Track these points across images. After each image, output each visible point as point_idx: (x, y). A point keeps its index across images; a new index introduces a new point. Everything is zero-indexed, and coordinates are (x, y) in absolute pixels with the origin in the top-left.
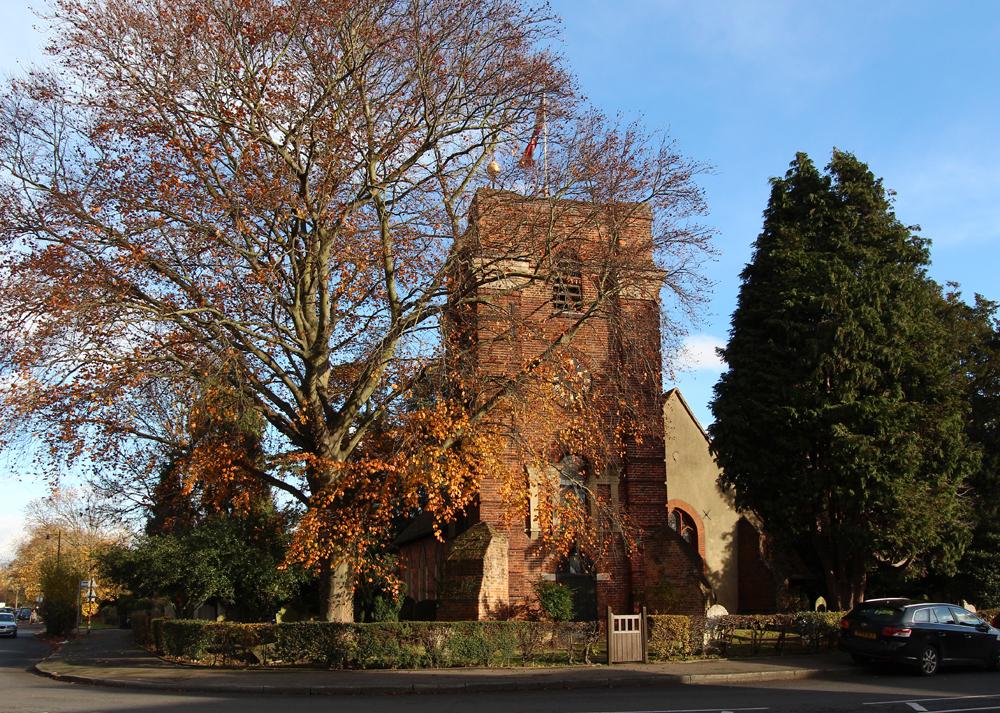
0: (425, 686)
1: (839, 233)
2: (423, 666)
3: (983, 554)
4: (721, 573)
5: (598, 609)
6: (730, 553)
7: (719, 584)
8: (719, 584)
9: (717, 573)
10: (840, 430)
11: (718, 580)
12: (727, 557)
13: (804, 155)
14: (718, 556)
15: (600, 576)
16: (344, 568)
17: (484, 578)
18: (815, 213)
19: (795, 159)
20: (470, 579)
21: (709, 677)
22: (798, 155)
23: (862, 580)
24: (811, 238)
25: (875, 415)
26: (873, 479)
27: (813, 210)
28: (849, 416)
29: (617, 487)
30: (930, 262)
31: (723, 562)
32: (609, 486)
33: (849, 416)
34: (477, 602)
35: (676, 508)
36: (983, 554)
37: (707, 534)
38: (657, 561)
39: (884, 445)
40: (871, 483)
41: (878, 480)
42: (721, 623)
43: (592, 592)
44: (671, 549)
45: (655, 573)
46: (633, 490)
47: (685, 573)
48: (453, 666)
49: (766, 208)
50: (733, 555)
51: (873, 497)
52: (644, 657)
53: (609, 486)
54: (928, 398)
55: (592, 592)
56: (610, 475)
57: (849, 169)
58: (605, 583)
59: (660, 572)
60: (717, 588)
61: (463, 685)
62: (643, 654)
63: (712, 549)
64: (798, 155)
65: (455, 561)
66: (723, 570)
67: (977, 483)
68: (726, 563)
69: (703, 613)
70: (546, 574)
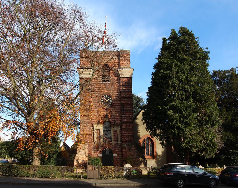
0: (15, 182)
1: (179, 53)
2: (33, 177)
3: (234, 151)
4: (161, 155)
5: (114, 164)
6: (164, 150)
7: (160, 158)
8: (160, 158)
9: (159, 156)
10: (170, 112)
11: (160, 157)
12: (163, 151)
13: (174, 30)
14: (160, 150)
15: (114, 155)
16: (36, 151)
17: (77, 155)
18: (173, 47)
19: (171, 31)
20: (74, 155)
21: (102, 184)
22: (172, 30)
23: (187, 158)
24: (172, 54)
25: (181, 107)
26: (178, 127)
27: (172, 46)
28: (174, 108)
29: (119, 130)
30: (209, 59)
31: (161, 152)
32: (117, 130)
33: (174, 108)
34: (74, 161)
35: (147, 137)
36: (234, 151)
37: (157, 144)
38: (130, 151)
39: (184, 117)
40: (178, 128)
41: (180, 127)
42: (129, 169)
43: (112, 159)
44: (133, 148)
45: (129, 155)
46: (123, 131)
47: (136, 155)
48: (41, 177)
49: (161, 47)
50: (165, 150)
51: (179, 132)
52: (99, 178)
53: (117, 130)
54: (201, 102)
55: (112, 159)
56: (117, 127)
57: (184, 32)
58: (116, 157)
59: (130, 154)
60: (160, 159)
61: (24, 183)
62: (99, 177)
63: (158, 148)
64: (172, 30)
65: (71, 150)
66: (162, 154)
67: (226, 127)
68: (163, 152)
69: (123, 166)
70: (99, 154)
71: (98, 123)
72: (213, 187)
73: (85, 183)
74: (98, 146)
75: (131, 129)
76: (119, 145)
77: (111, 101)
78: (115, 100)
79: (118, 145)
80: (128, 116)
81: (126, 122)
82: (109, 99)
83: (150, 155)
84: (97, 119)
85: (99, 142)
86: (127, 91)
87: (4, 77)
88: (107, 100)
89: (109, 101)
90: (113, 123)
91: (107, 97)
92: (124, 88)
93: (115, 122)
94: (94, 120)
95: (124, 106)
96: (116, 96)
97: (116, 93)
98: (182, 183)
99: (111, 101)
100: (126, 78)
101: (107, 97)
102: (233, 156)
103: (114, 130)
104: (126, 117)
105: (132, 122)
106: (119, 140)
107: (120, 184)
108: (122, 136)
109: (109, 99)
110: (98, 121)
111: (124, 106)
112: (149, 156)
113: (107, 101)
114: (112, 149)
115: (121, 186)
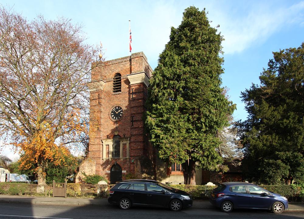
15: (123, 172)
29: (128, 144)
43: (120, 176)
58: (124, 174)
71: (108, 137)
72: (173, 208)
73: (294, 203)
74: (107, 162)
75: (140, 141)
76: (128, 160)
77: (121, 112)
78: (126, 110)
79: (127, 160)
80: (138, 127)
81: (136, 134)
82: (119, 111)
83: (181, 171)
84: (107, 134)
85: (108, 158)
86: (137, 99)
87: (165, 91)
88: (117, 112)
89: (119, 113)
90: (123, 136)
91: (117, 108)
92: (134, 96)
93: (124, 135)
94: (103, 135)
95: (133, 116)
96: (126, 107)
97: (127, 104)
98: (127, 204)
99: (121, 112)
100: (136, 85)
101: (117, 108)
102: (267, 168)
103: (123, 144)
104: (135, 128)
105: (141, 134)
106: (128, 155)
107: (61, 203)
108: (131, 149)
109: (119, 111)
110: (108, 136)
111: (133, 116)
112: (180, 172)
113: (117, 113)
114: (120, 165)
115: (62, 205)
